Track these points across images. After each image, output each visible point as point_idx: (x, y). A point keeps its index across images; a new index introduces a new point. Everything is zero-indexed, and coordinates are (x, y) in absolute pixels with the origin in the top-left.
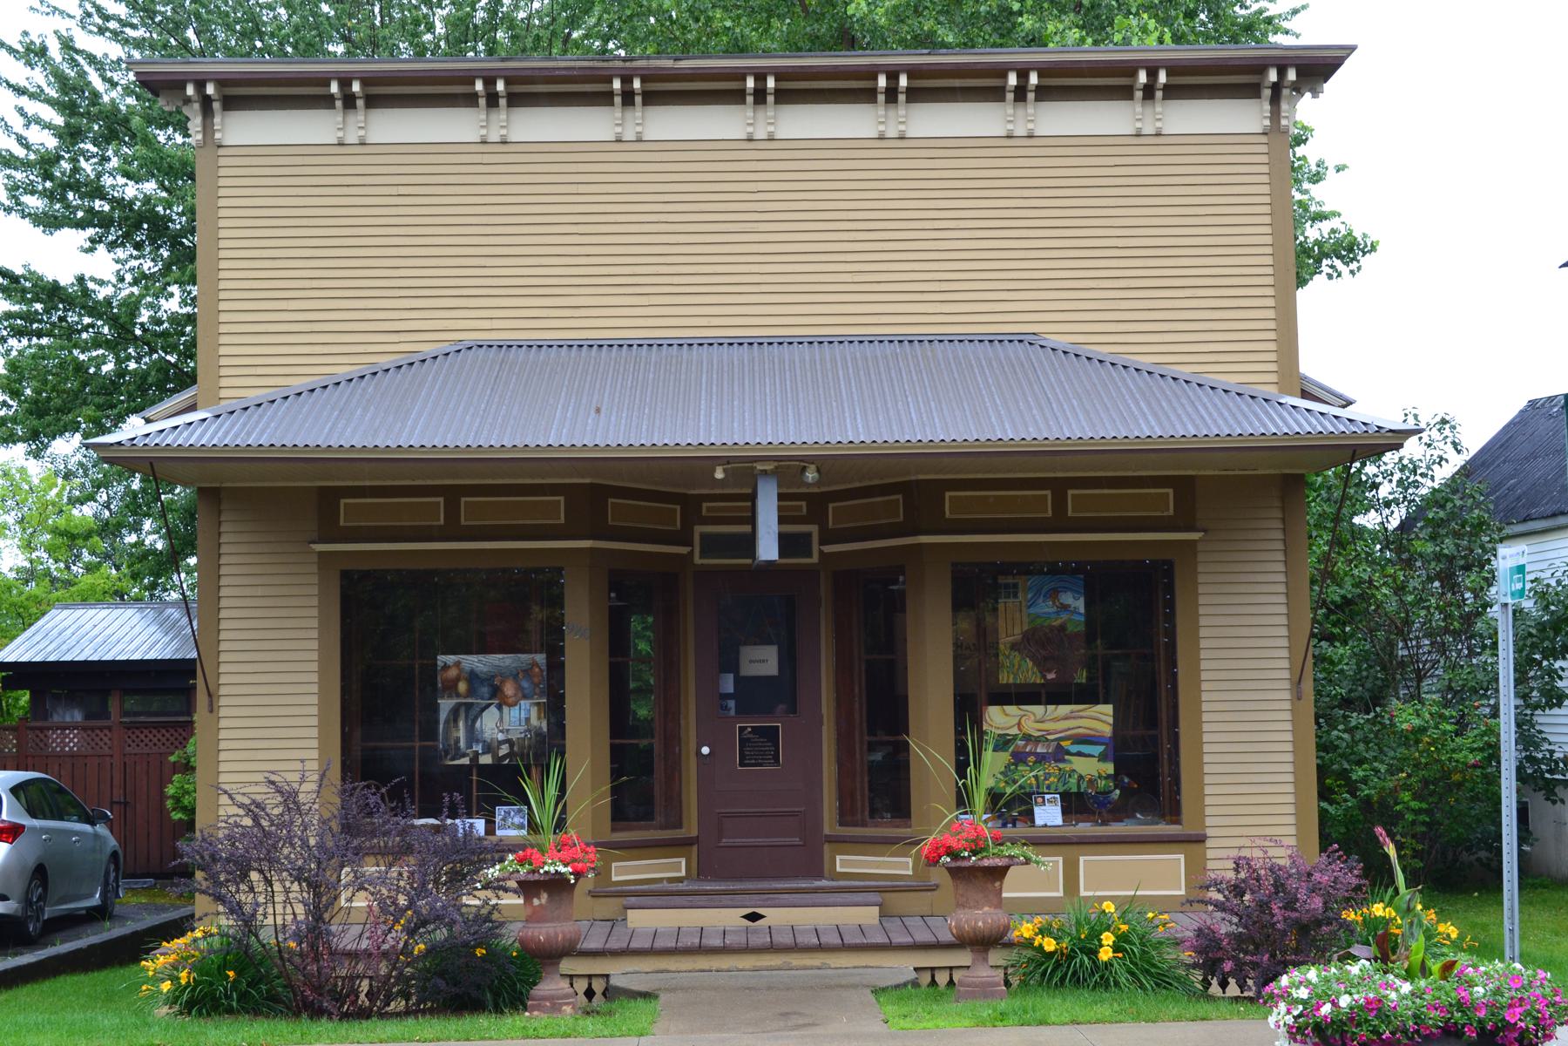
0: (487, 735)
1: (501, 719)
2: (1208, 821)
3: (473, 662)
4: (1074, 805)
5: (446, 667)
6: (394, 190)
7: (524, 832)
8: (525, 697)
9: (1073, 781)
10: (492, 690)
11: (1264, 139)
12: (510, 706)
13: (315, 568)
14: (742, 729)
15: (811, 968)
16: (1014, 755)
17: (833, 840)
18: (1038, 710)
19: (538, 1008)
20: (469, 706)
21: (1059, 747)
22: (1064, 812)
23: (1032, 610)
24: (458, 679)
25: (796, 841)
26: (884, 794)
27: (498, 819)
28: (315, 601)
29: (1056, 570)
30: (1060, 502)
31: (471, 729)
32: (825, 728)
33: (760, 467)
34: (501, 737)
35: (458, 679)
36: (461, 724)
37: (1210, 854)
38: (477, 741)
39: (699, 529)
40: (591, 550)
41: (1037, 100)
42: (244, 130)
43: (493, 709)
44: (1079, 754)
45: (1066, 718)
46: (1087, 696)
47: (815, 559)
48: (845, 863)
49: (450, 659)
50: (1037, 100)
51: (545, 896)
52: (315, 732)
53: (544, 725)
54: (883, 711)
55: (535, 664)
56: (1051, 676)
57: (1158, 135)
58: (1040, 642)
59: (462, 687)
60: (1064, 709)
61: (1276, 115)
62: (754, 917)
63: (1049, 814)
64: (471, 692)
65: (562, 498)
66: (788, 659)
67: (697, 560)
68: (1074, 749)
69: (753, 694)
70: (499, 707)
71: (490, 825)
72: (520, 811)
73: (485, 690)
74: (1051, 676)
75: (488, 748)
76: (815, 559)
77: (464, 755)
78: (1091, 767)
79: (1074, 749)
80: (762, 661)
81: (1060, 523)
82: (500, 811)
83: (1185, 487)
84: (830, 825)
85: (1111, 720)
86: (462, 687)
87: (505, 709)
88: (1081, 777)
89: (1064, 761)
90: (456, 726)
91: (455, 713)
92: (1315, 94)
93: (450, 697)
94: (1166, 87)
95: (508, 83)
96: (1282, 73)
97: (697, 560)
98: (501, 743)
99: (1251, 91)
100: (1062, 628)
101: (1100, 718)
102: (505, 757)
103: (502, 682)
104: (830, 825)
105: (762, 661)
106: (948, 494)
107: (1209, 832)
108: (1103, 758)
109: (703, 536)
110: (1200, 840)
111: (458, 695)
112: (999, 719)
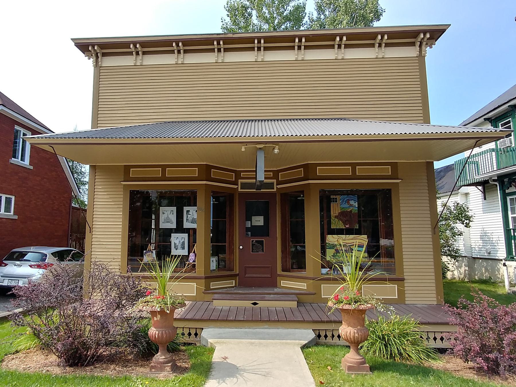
14: (252, 241)
16: (336, 250)
17: (279, 276)
18: (343, 236)
23: (342, 206)
25: (269, 276)
26: (297, 261)
29: (350, 193)
30: (354, 170)
32: (278, 241)
37: (406, 285)
46: (358, 232)
47: (275, 190)
48: (284, 283)
54: (296, 235)
56: (347, 226)
58: (344, 215)
60: (352, 236)
61: (420, 51)
62: (255, 304)
66: (266, 221)
67: (240, 190)
69: (255, 231)
76: (275, 190)
80: (259, 221)
84: (279, 271)
92: (431, 47)
95: (184, 45)
96: (425, 35)
97: (240, 190)
100: (351, 211)
101: (363, 240)
104: (279, 271)
105: (259, 221)
106: (318, 167)
110: (403, 280)
112: (331, 239)
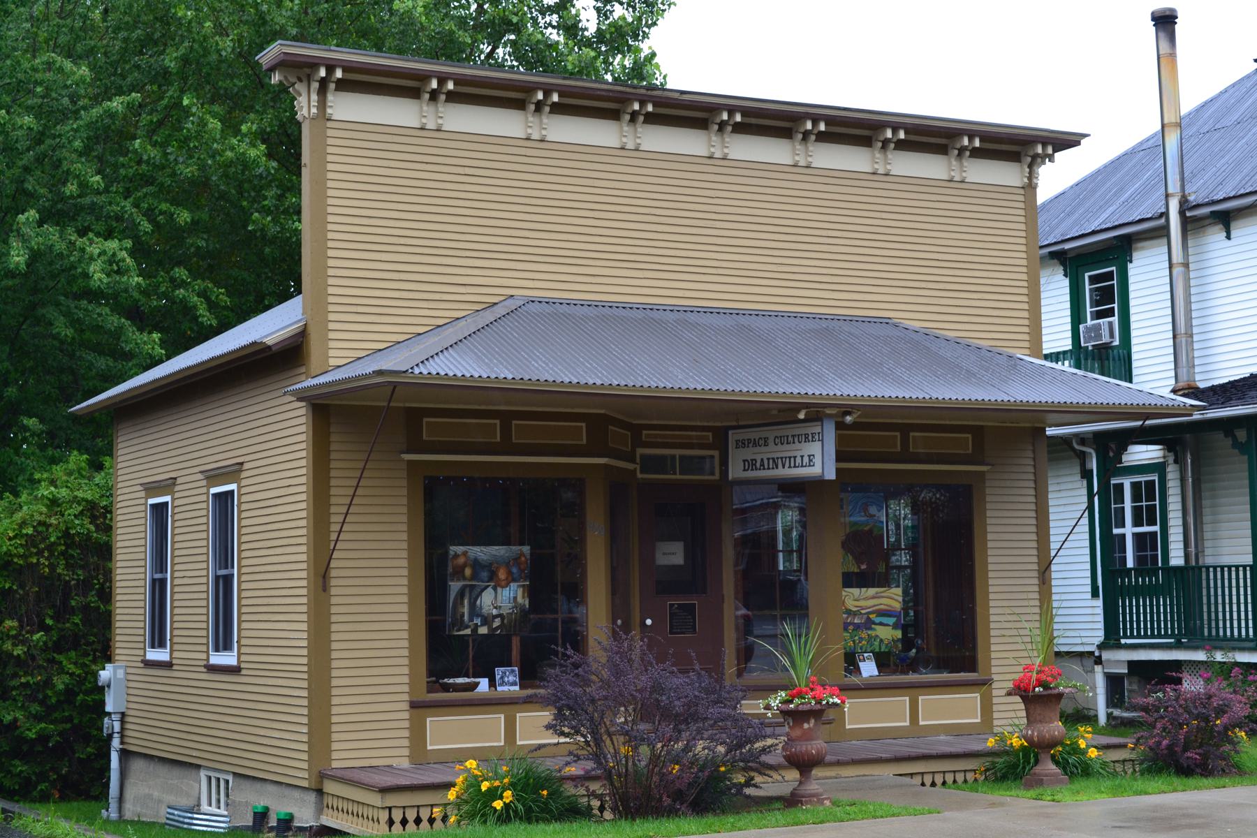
0: (485, 611)
1: (496, 597)
2: (994, 670)
3: (481, 552)
4: (883, 661)
5: (456, 556)
6: (461, 170)
7: (517, 688)
8: (514, 580)
9: (877, 643)
10: (488, 574)
11: (1022, 191)
12: (502, 587)
13: (405, 474)
15: (831, 778)
19: (809, 802)
20: (472, 587)
21: (868, 618)
22: (878, 667)
24: (465, 565)
27: (498, 677)
28: (405, 501)
31: (473, 605)
33: (828, 411)
34: (495, 612)
35: (465, 565)
36: (466, 602)
38: (478, 616)
39: (640, 451)
40: (605, 466)
41: (336, 89)
42: (349, 108)
43: (490, 590)
44: (881, 624)
45: (873, 598)
49: (460, 549)
50: (336, 89)
51: (813, 721)
52: (405, 608)
53: (527, 603)
55: (522, 554)
56: (864, 567)
57: (962, 182)
59: (468, 572)
60: (872, 591)
63: (869, 669)
64: (474, 577)
65: (498, 422)
67: (639, 476)
68: (878, 620)
70: (495, 589)
71: (492, 684)
72: (513, 671)
73: (485, 574)
74: (864, 567)
75: (486, 620)
77: (467, 627)
78: (887, 633)
79: (878, 620)
80: (672, 554)
81: (507, 447)
82: (499, 671)
83: (978, 432)
85: (900, 599)
86: (468, 572)
87: (499, 590)
88: (881, 640)
89: (870, 629)
90: (462, 604)
91: (461, 594)
93: (458, 580)
94: (339, 81)
98: (495, 617)
99: (1014, 157)
102: (497, 628)
103: (498, 568)
105: (672, 554)
107: (995, 677)
108: (895, 627)
109: (642, 456)
111: (464, 579)
